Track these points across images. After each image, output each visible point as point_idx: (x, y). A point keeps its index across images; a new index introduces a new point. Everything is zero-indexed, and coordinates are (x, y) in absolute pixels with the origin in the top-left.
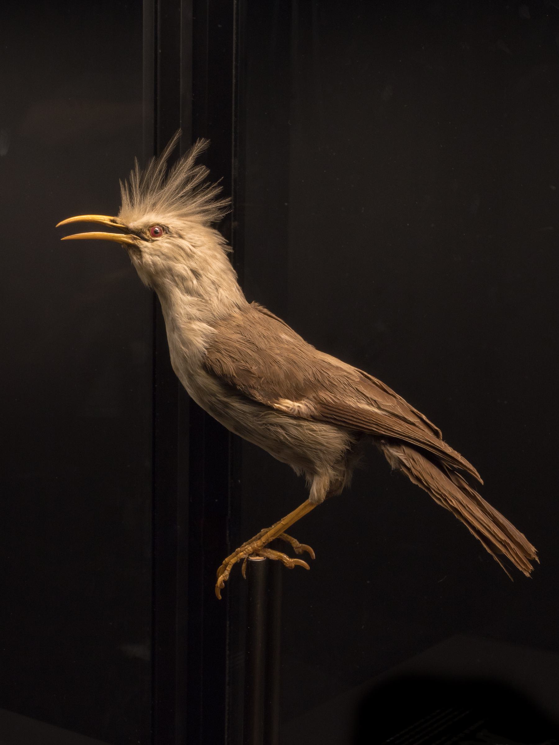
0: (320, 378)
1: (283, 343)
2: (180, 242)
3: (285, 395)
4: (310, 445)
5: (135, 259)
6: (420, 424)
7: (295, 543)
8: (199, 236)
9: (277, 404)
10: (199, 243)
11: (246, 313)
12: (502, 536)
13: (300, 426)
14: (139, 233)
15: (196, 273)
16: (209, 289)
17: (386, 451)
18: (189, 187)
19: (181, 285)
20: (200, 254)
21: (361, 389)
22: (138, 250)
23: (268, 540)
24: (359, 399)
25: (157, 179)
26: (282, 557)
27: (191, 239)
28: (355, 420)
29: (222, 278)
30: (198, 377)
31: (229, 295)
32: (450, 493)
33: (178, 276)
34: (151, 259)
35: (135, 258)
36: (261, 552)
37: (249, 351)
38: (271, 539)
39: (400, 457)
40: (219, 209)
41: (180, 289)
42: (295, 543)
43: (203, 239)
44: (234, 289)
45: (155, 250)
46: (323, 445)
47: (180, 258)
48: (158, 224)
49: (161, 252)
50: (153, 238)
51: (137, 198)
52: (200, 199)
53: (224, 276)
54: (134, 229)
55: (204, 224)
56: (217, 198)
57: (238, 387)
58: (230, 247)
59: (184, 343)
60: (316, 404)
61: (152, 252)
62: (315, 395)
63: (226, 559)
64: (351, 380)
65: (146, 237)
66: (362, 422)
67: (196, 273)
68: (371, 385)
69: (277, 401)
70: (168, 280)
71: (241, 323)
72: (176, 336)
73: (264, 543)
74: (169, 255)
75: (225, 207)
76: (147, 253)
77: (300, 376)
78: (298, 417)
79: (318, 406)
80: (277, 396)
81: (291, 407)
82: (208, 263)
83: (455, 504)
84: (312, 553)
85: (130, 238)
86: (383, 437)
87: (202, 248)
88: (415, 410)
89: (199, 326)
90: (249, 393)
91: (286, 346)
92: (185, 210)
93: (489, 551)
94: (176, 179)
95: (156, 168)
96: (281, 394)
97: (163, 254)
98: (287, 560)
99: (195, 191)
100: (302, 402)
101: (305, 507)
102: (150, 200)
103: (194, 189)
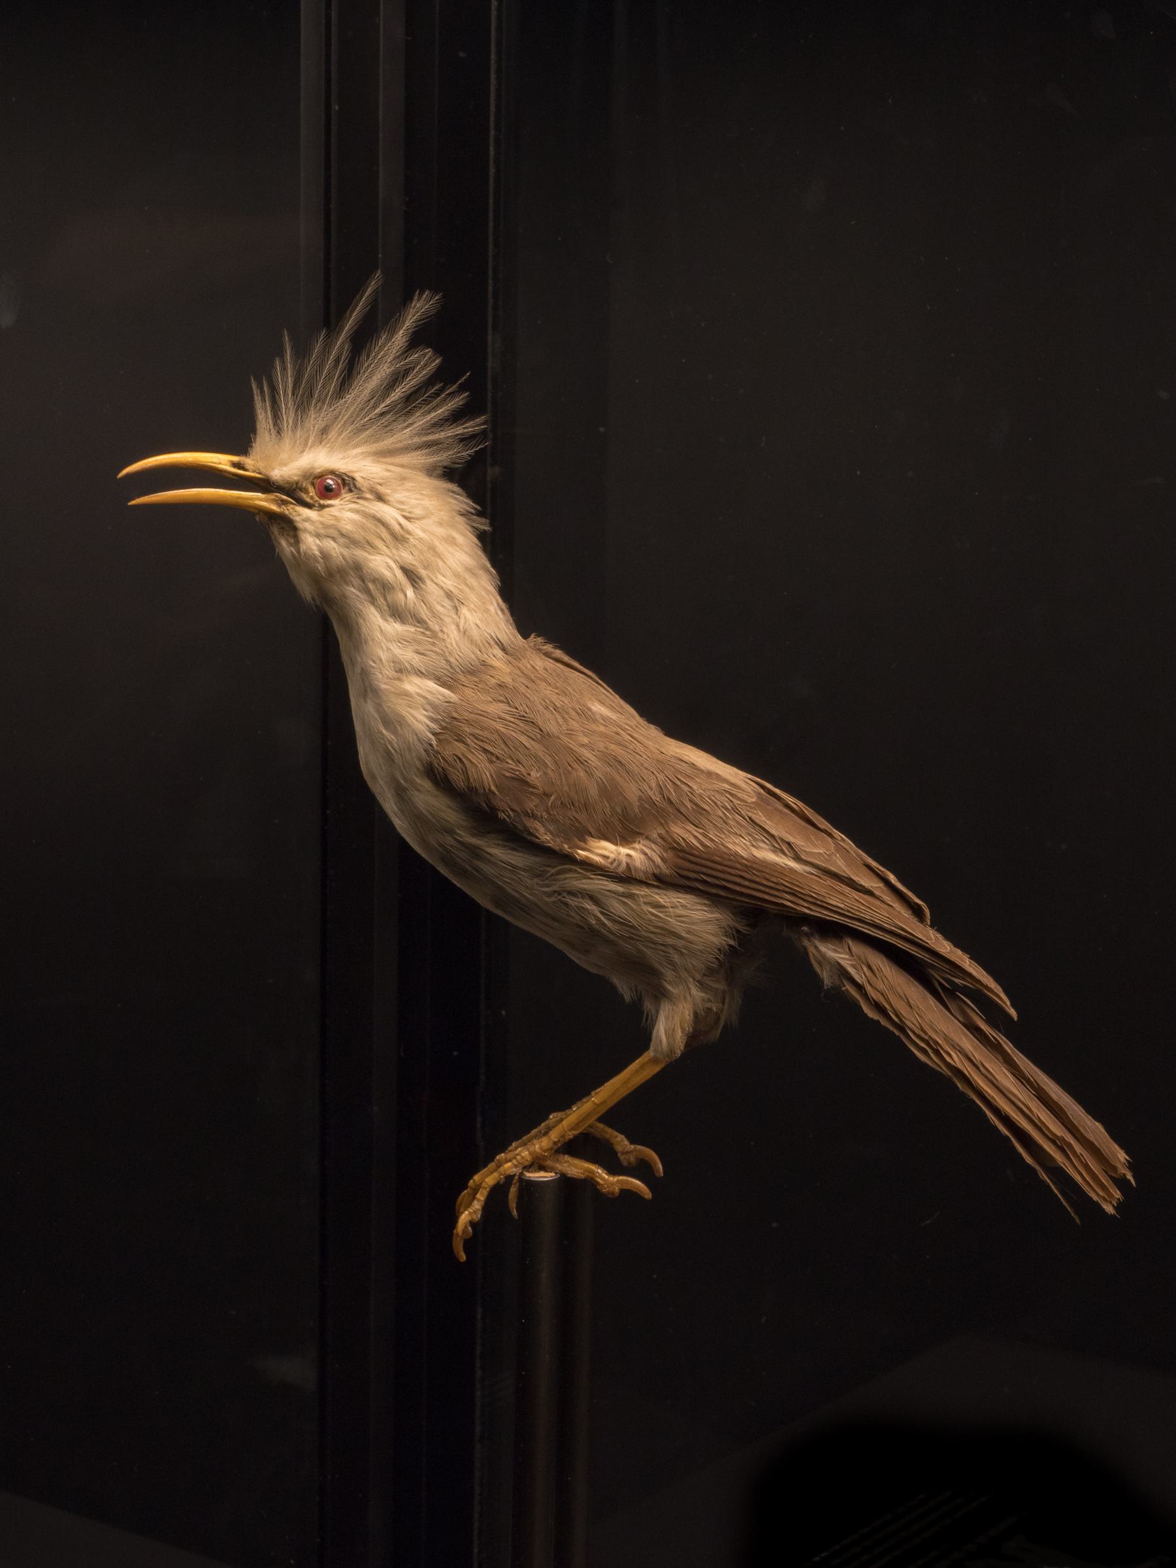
0: (674, 796)
1: (596, 722)
2: (379, 509)
3: (599, 831)
4: (651, 936)
5: (285, 546)
6: (883, 892)
7: (621, 1143)
8: (418, 496)
9: (583, 849)
10: (418, 512)
11: (517, 659)
12: (1057, 1129)
13: (631, 896)
14: (291, 491)
15: (411, 575)
16: (439, 608)
17: (811, 950)
18: (397, 394)
19: (381, 601)
20: (421, 534)
21: (760, 818)
22: (289, 526)
23: (563, 1136)
24: (755, 840)
25: (330, 377)
26: (592, 1172)
27: (402, 503)
28: (746, 883)
29: (467, 585)
30: (416, 793)
31: (481, 620)
32: (946, 1039)
33: (374, 581)
34: (318, 546)
35: (284, 543)
36: (549, 1163)
37: (523, 739)
38: (570, 1135)
39: (842, 962)
40: (462, 440)
41: (378, 608)
42: (621, 1143)
43: (427, 502)
44: (492, 609)
45: (326, 527)
46: (680, 937)
47: (379, 544)
48: (333, 472)
49: (339, 531)
50: (322, 502)
51: (288, 417)
52: (421, 420)
53: (472, 581)
54: (281, 483)
55: (430, 471)
56: (456, 417)
57: (502, 815)
58: (483, 520)
59: (387, 722)
60: (666, 851)
61: (319, 531)
62: (663, 832)
63: (476, 1177)
64: (739, 799)
65: (308, 500)
66: (762, 888)
67: (411, 575)
68: (780, 811)
69: (582, 844)
70: (353, 590)
71: (508, 680)
72: (370, 707)
73: (555, 1143)
74: (356, 536)
75: (473, 436)
76: (310, 533)
77: (632, 792)
78: (627, 877)
79: (669, 855)
80: (582, 834)
81: (612, 856)
82: (437, 554)
83: (957, 1060)
84: (656, 1164)
85: (274, 501)
86: (805, 919)
87: (425, 521)
88: (874, 864)
89: (418, 686)
90: (525, 827)
91: (602, 729)
92: (388, 442)
93: (1029, 1160)
94: (370, 377)
95: (329, 353)
96: (591, 830)
97: (343, 535)
98: (603, 1179)
99: (410, 403)
100: (636, 845)
101: (642, 1067)
102: (315, 420)
103: (409, 399)
